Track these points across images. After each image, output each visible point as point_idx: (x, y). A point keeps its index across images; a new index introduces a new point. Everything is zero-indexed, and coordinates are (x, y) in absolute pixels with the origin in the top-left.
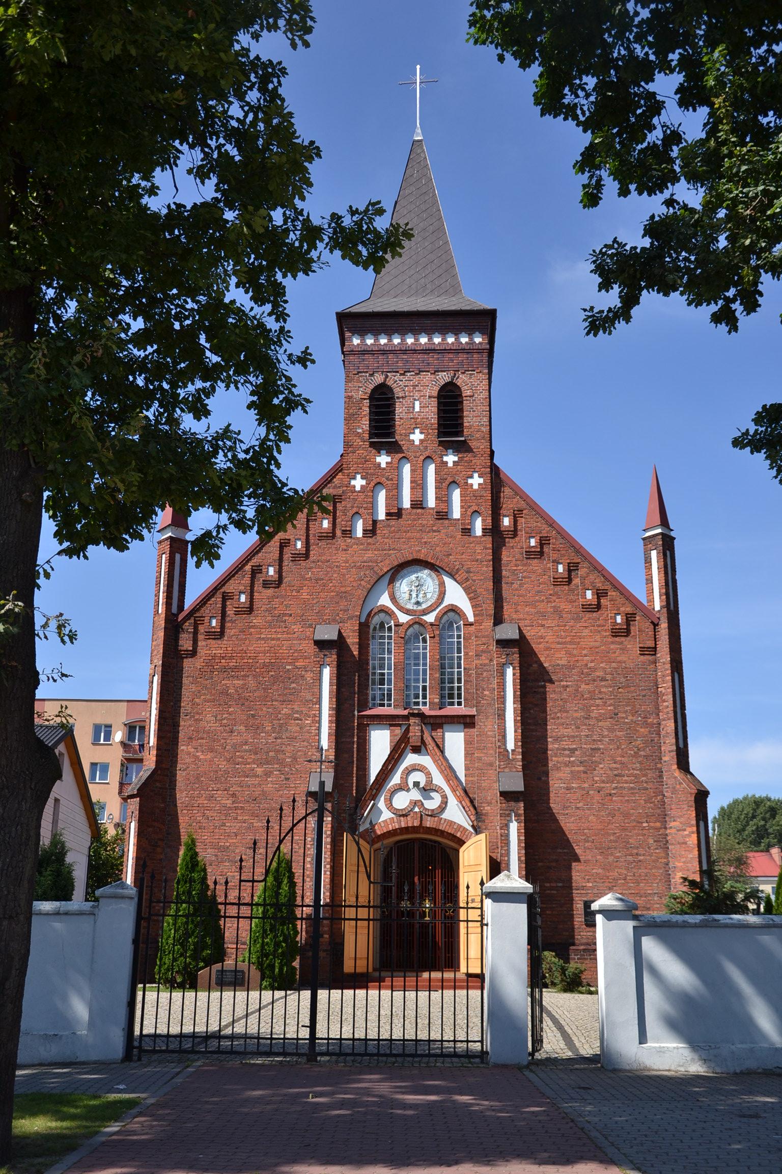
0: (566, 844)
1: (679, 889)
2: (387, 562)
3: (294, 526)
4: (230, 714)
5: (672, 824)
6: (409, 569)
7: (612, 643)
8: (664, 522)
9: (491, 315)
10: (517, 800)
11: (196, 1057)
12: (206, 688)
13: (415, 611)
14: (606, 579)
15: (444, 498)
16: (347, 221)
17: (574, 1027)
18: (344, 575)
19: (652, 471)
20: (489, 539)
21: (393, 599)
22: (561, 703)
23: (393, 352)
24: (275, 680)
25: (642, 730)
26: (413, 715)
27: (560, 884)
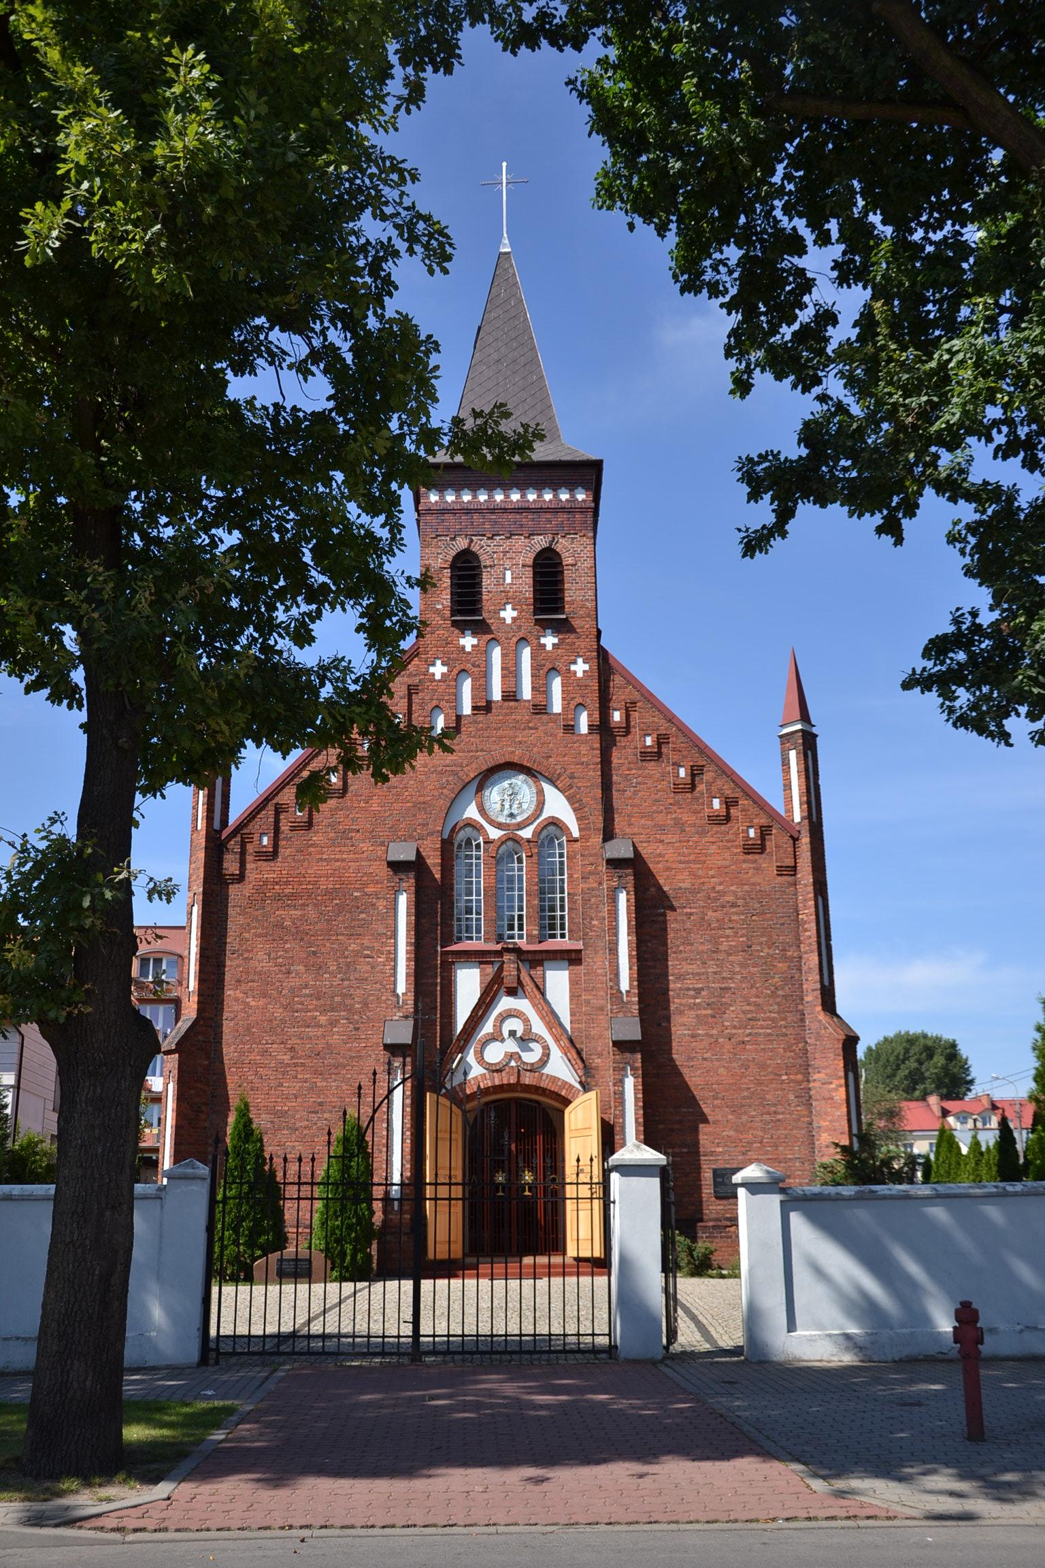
0: (692, 1101)
1: (831, 1156)
2: (474, 766)
3: (413, 767)
4: (286, 951)
5: (816, 1076)
6: (501, 774)
7: (744, 861)
8: (805, 717)
9: (596, 467)
10: (633, 1051)
11: (281, 1359)
12: (257, 921)
13: (509, 825)
14: (737, 785)
15: (541, 688)
16: (469, 424)
17: (709, 1317)
18: (422, 782)
19: (790, 655)
20: (596, 737)
21: (482, 810)
22: (684, 934)
23: (479, 511)
24: (340, 909)
25: (780, 965)
26: (508, 950)
27: (685, 1150)
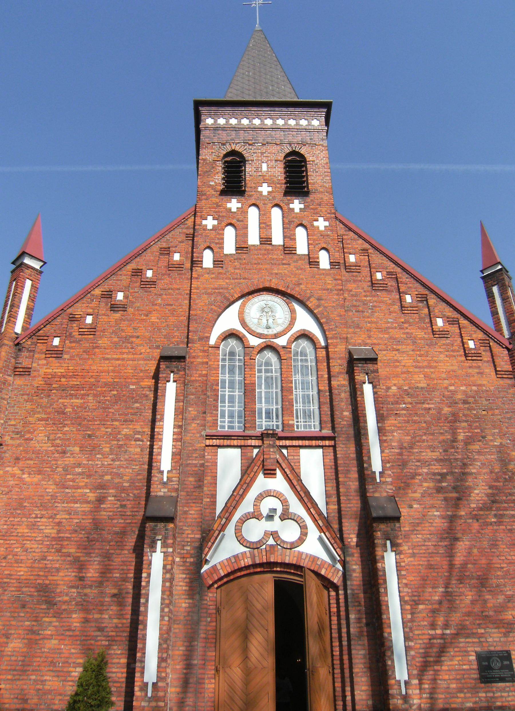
4: (64, 434)
24: (117, 399)
